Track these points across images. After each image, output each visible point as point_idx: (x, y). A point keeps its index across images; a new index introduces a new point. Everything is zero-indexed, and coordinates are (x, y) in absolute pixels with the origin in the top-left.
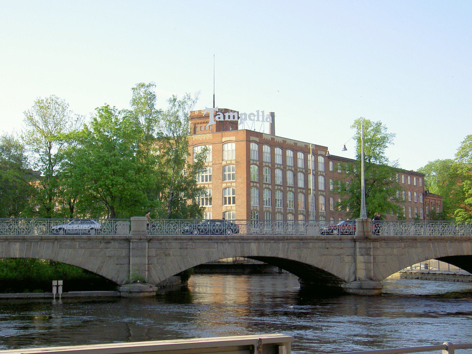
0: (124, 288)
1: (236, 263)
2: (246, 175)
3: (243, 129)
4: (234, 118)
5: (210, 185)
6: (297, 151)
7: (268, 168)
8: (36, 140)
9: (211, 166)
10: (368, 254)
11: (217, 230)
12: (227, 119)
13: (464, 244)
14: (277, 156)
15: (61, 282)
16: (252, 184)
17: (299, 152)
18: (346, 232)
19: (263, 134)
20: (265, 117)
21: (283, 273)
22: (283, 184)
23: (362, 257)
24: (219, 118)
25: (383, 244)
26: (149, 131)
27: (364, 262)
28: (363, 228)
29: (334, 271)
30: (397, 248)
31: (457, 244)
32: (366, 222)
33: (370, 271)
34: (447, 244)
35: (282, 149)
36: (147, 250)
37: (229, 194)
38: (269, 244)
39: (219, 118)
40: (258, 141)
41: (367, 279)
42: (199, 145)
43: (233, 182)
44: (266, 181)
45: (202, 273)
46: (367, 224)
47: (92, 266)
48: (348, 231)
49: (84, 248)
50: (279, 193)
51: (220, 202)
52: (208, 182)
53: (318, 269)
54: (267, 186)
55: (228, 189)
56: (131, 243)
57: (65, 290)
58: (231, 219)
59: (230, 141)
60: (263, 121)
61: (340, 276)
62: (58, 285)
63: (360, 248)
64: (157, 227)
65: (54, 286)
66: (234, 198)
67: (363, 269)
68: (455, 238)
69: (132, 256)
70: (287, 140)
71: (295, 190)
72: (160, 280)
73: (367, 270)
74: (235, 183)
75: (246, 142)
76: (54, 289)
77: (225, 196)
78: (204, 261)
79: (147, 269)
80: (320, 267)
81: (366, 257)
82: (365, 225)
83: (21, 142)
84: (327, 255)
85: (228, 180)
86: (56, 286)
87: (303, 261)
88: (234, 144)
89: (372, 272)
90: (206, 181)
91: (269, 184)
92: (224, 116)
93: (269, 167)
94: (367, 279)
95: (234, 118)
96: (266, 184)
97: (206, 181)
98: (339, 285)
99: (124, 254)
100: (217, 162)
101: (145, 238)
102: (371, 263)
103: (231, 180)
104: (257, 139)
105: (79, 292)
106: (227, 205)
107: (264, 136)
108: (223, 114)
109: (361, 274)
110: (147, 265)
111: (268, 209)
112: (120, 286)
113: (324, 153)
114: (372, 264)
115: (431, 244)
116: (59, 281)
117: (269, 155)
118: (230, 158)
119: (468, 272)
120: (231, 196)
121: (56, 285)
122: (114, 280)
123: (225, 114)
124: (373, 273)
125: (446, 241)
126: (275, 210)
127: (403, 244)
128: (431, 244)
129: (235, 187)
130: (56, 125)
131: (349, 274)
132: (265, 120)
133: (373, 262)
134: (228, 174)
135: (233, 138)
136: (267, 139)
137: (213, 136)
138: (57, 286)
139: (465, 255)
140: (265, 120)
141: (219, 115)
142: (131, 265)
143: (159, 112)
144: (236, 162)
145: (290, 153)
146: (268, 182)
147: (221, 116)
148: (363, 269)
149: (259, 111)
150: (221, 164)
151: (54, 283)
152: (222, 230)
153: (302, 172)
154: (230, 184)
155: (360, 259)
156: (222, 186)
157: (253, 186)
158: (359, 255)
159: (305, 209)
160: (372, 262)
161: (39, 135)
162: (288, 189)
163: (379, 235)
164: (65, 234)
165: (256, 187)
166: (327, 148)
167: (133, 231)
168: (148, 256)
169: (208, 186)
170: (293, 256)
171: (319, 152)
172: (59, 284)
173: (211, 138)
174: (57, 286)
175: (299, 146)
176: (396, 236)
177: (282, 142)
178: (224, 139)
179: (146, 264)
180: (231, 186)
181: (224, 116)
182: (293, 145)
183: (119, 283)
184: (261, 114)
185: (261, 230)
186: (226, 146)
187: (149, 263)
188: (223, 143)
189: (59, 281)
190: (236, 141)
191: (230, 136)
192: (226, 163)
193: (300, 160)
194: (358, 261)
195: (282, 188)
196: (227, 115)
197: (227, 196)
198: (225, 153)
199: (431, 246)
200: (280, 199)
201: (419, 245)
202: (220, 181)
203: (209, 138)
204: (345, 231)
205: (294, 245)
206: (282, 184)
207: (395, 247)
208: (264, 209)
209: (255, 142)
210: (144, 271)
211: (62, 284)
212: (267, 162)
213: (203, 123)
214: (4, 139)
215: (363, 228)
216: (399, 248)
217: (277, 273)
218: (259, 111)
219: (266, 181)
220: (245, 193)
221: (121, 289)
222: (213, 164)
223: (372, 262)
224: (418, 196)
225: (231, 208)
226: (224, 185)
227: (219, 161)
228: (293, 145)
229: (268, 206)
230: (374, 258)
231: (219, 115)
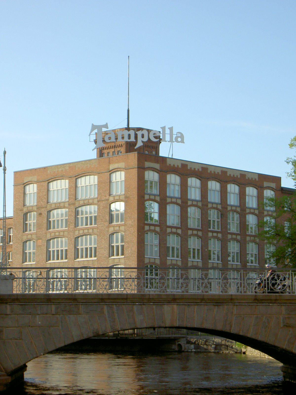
1: (119, 338)
2: (136, 215)
5: (94, 230)
6: (227, 182)
7: (216, 211)
9: (95, 204)
13: (167, 308)
14: (193, 189)
16: (147, 228)
17: (230, 183)
19: (167, 159)
20: (174, 136)
21: (183, 351)
22: (202, 227)
25: (17, 308)
30: (43, 314)
31: (154, 307)
35: (200, 180)
37: (117, 242)
40: (159, 169)
42: (82, 175)
44: (214, 228)
45: (88, 352)
50: (215, 242)
51: (106, 253)
52: (93, 226)
55: (116, 235)
58: (119, 277)
59: (118, 168)
60: (171, 141)
66: (123, 246)
68: (147, 297)
70: (246, 173)
71: (223, 236)
74: (123, 227)
75: (137, 169)
77: (112, 245)
78: (87, 333)
85: (116, 222)
88: (123, 173)
90: (91, 224)
91: (217, 232)
96: (213, 232)
97: (91, 224)
103: (119, 223)
104: (157, 166)
106: (115, 257)
107: (168, 162)
111: (174, 262)
113: (273, 185)
117: (177, 188)
118: (119, 193)
120: (120, 244)
125: (133, 302)
126: (187, 264)
127: (53, 307)
128: (105, 308)
129: (124, 232)
132: (174, 140)
135: (122, 165)
136: (195, 169)
139: (232, 332)
140: (174, 140)
144: (126, 197)
145: (214, 185)
146: (216, 230)
149: (164, 127)
150: (108, 200)
153: (253, 213)
154: (117, 228)
156: (108, 231)
157: (150, 230)
159: (240, 263)
162: (210, 234)
165: (154, 231)
166: (281, 178)
169: (93, 231)
171: (266, 184)
175: (211, 171)
176: (187, 293)
178: (112, 167)
180: (120, 230)
182: (239, 177)
184: (168, 131)
186: (114, 175)
188: (111, 172)
190: (125, 169)
193: (232, 195)
197: (114, 244)
198: (114, 186)
200: (175, 246)
201: (82, 308)
202: (107, 224)
206: (200, 228)
207: (39, 313)
212: (215, 203)
213: (107, 149)
216: (46, 314)
217: (176, 351)
218: (164, 127)
220: (135, 240)
222: (98, 201)
226: (111, 230)
227: (105, 196)
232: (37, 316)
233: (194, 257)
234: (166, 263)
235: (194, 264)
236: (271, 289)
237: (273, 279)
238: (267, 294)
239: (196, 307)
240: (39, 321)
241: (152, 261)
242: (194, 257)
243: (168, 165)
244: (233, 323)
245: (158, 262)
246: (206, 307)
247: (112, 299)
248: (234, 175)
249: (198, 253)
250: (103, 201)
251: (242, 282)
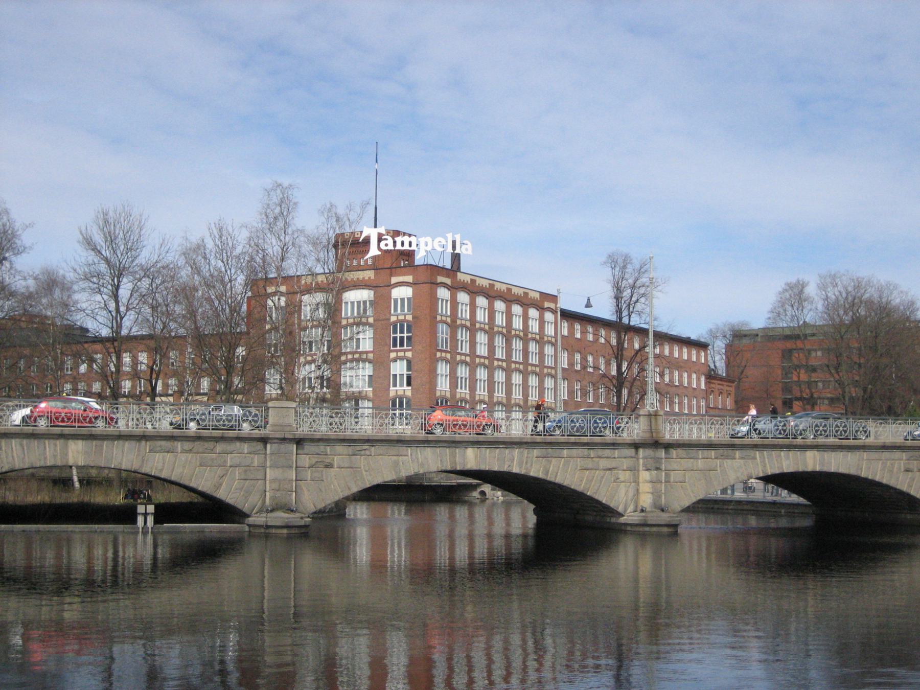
0: (257, 519)
3: (425, 263)
4: (410, 245)
8: (99, 275)
10: (658, 469)
11: (63, 418)
12: (399, 247)
13: (810, 454)
15: (151, 508)
18: (224, 425)
23: (647, 473)
24: (386, 245)
26: (68, 298)
27: (651, 482)
28: (651, 426)
29: (603, 497)
30: (704, 458)
32: (656, 415)
33: (660, 497)
34: (782, 453)
36: (294, 456)
38: (497, 451)
39: (386, 245)
40: (450, 284)
41: (654, 510)
43: (409, 350)
44: (462, 350)
46: (656, 419)
47: (204, 482)
48: (226, 423)
49: (190, 451)
53: (575, 492)
54: (463, 358)
56: (268, 446)
57: (157, 521)
61: (612, 505)
62: (146, 511)
63: (643, 458)
64: (841, 429)
65: (139, 514)
67: (648, 493)
69: (270, 467)
72: (315, 507)
73: (656, 494)
76: (140, 520)
79: (294, 489)
80: (580, 489)
81: (654, 473)
82: (653, 420)
83: (70, 276)
84: (591, 469)
86: (142, 514)
87: (550, 478)
89: (663, 497)
91: (466, 355)
92: (395, 242)
93: (467, 328)
94: (654, 510)
95: (410, 245)
96: (461, 354)
98: (608, 520)
99: (256, 464)
100: (383, 317)
101: (291, 437)
102: (661, 482)
103: (405, 347)
104: (448, 281)
105: (181, 525)
108: (393, 239)
109: (646, 500)
110: (294, 482)
111: (463, 395)
112: (248, 516)
113: (552, 306)
114: (663, 485)
115: (757, 452)
116: (148, 506)
119: (804, 500)
121: (144, 512)
122: (239, 506)
123: (395, 239)
124: (665, 498)
130: (129, 250)
131: (626, 500)
133: (666, 482)
134: (400, 337)
135: (409, 279)
136: (464, 281)
137: (376, 275)
138: (145, 515)
141: (386, 239)
142: (268, 482)
143: (302, 231)
146: (464, 351)
147: (390, 241)
148: (648, 493)
151: (141, 509)
152: (73, 418)
155: (645, 475)
158: (643, 470)
160: (663, 481)
161: (103, 267)
162: (496, 363)
163: (485, 434)
164: (51, 426)
167: (272, 426)
168: (296, 467)
170: (536, 470)
171: (547, 305)
172: (148, 512)
173: (373, 278)
174: (145, 515)
177: (488, 286)
179: (292, 480)
181: (395, 242)
182: (505, 291)
183: (246, 509)
185: (460, 428)
187: (298, 478)
189: (148, 506)
191: (404, 275)
192: (398, 318)
194: (641, 480)
195: (487, 362)
196: (399, 240)
199: (758, 456)
201: (738, 454)
203: (370, 278)
204: (221, 423)
205: (536, 452)
208: (458, 396)
209: (444, 285)
210: (289, 493)
211: (153, 511)
214: (328, 206)
215: (651, 426)
219: (462, 350)
221: (251, 520)
223: (663, 481)
224: (698, 379)
225: (404, 392)
227: (385, 315)
228: (505, 291)
229: (463, 391)
230: (667, 475)
231: (386, 239)
232: (699, 460)
233: (461, 388)
234: (456, 395)
235: (442, 394)
236: (593, 433)
237: (821, 435)
238: (566, 437)
239: (488, 450)
240: (700, 464)
241: (443, 394)
242: (461, 388)
243: (458, 280)
244: (760, 465)
245: (448, 395)
246: (842, 453)
247: (348, 439)
248: (464, 281)
249: (466, 381)
250: (381, 320)
251: (611, 425)
